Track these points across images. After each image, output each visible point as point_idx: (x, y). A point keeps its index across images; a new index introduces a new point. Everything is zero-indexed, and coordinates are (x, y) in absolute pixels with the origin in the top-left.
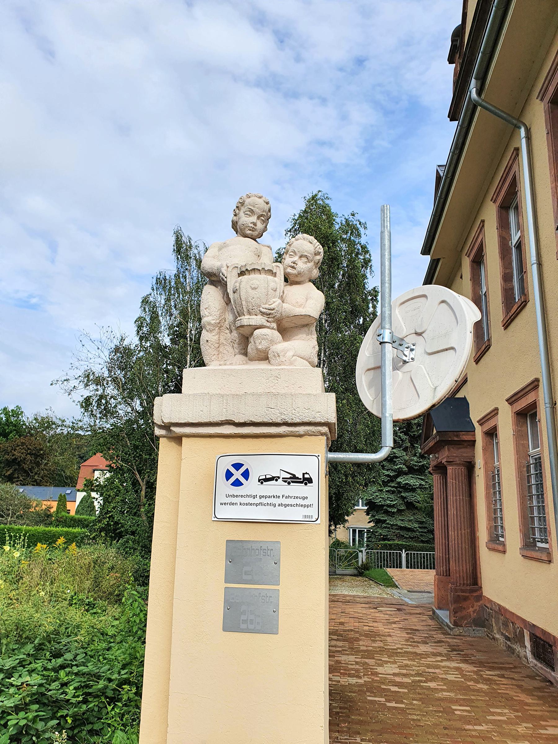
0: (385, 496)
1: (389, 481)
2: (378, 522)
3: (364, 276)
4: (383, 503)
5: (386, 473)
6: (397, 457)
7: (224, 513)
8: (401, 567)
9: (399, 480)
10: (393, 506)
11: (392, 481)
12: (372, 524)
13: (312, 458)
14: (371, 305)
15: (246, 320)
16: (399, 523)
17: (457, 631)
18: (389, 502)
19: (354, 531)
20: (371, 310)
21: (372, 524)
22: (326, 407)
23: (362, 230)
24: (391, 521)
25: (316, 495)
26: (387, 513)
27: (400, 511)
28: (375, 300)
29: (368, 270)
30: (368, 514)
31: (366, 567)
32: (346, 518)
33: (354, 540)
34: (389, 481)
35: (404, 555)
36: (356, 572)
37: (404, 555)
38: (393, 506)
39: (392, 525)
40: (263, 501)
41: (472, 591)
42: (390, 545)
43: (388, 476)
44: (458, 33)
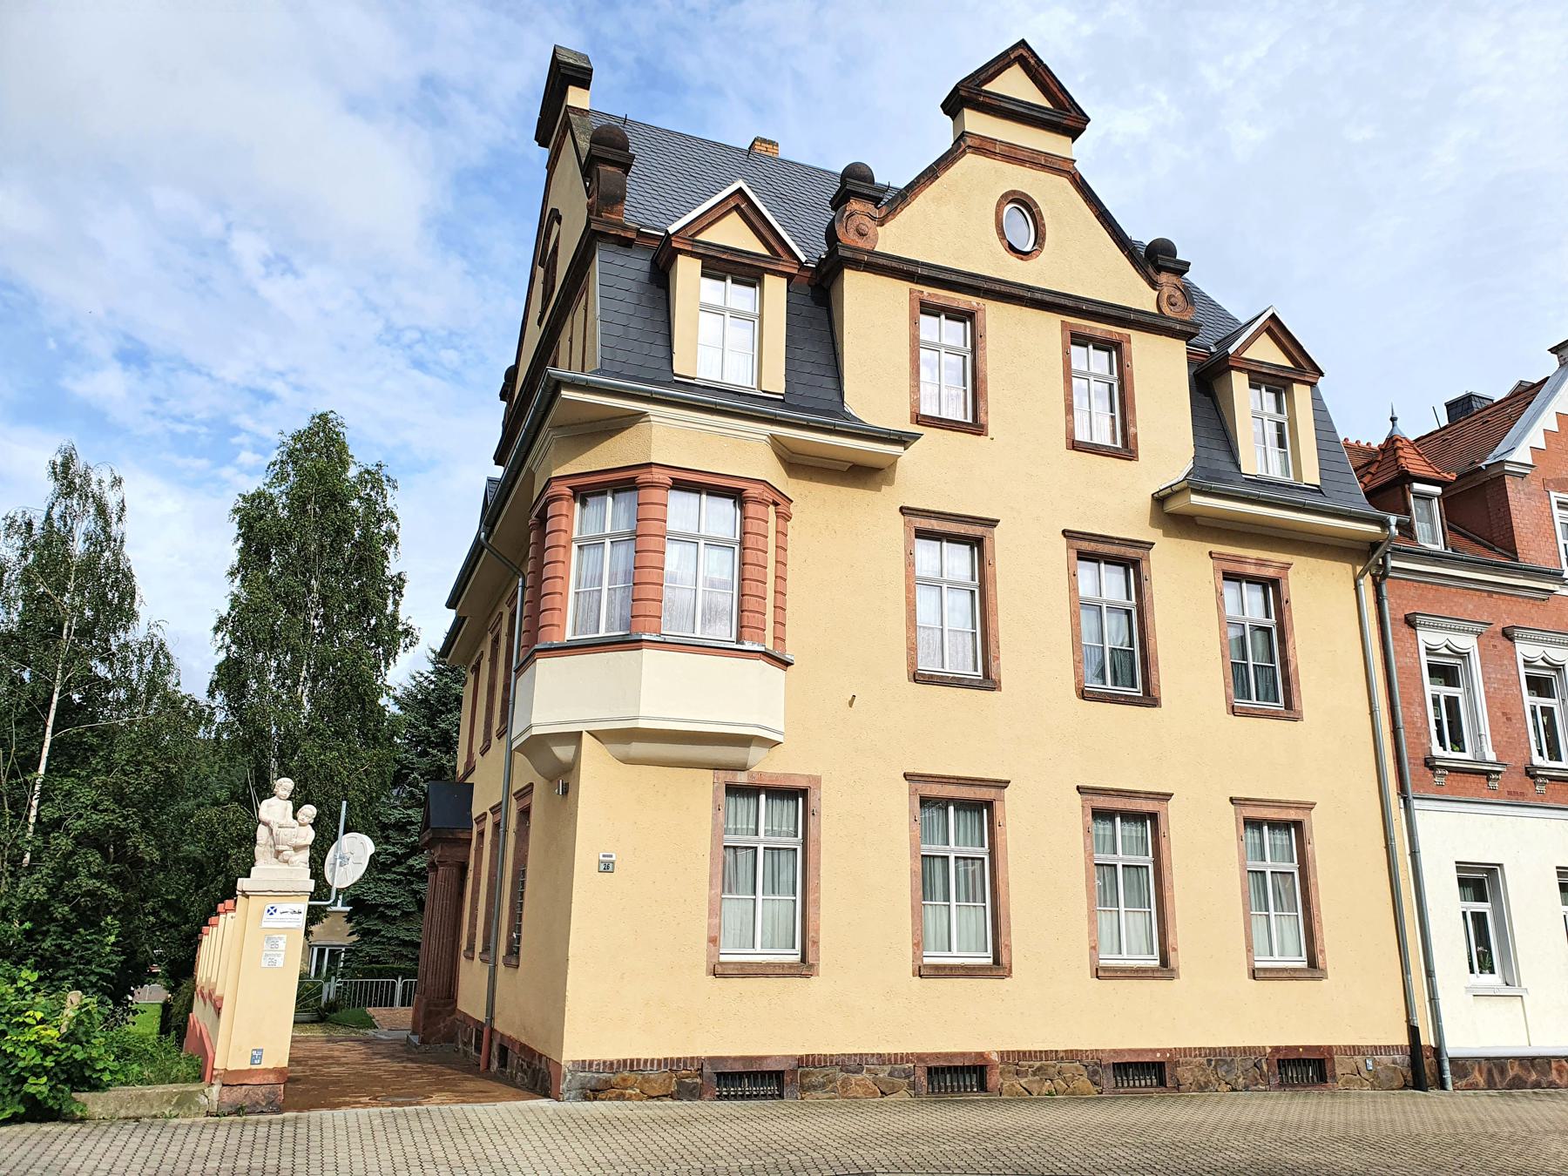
0: (383, 888)
1: (393, 864)
2: (365, 934)
3: (385, 555)
4: (379, 900)
5: (391, 849)
6: (412, 823)
7: (264, 925)
8: (392, 1005)
9: (411, 862)
10: (394, 907)
11: (400, 864)
12: (355, 938)
13: (303, 905)
14: (390, 602)
15: (280, 848)
16: (403, 935)
17: (423, 1048)
18: (388, 900)
19: (321, 953)
20: (390, 608)
21: (355, 938)
22: (311, 885)
23: (389, 491)
24: (388, 931)
25: (303, 918)
26: (383, 917)
27: (406, 915)
28: (398, 591)
29: (392, 549)
30: (349, 921)
31: (332, 1007)
32: (309, 811)
33: (318, 968)
34: (393, 864)
35: (399, 985)
36: (315, 1017)
37: (399, 985)
38: (394, 907)
39: (390, 939)
40: (282, 920)
41: (446, 1005)
42: (379, 970)
43: (394, 854)
44: (511, 374)
